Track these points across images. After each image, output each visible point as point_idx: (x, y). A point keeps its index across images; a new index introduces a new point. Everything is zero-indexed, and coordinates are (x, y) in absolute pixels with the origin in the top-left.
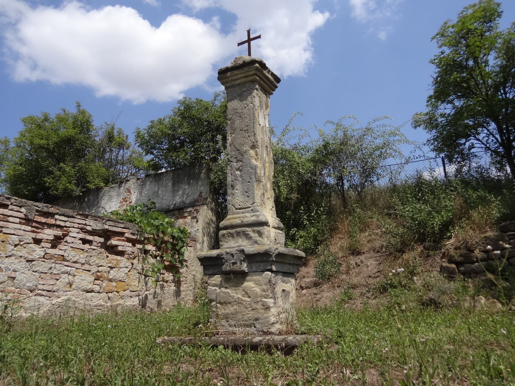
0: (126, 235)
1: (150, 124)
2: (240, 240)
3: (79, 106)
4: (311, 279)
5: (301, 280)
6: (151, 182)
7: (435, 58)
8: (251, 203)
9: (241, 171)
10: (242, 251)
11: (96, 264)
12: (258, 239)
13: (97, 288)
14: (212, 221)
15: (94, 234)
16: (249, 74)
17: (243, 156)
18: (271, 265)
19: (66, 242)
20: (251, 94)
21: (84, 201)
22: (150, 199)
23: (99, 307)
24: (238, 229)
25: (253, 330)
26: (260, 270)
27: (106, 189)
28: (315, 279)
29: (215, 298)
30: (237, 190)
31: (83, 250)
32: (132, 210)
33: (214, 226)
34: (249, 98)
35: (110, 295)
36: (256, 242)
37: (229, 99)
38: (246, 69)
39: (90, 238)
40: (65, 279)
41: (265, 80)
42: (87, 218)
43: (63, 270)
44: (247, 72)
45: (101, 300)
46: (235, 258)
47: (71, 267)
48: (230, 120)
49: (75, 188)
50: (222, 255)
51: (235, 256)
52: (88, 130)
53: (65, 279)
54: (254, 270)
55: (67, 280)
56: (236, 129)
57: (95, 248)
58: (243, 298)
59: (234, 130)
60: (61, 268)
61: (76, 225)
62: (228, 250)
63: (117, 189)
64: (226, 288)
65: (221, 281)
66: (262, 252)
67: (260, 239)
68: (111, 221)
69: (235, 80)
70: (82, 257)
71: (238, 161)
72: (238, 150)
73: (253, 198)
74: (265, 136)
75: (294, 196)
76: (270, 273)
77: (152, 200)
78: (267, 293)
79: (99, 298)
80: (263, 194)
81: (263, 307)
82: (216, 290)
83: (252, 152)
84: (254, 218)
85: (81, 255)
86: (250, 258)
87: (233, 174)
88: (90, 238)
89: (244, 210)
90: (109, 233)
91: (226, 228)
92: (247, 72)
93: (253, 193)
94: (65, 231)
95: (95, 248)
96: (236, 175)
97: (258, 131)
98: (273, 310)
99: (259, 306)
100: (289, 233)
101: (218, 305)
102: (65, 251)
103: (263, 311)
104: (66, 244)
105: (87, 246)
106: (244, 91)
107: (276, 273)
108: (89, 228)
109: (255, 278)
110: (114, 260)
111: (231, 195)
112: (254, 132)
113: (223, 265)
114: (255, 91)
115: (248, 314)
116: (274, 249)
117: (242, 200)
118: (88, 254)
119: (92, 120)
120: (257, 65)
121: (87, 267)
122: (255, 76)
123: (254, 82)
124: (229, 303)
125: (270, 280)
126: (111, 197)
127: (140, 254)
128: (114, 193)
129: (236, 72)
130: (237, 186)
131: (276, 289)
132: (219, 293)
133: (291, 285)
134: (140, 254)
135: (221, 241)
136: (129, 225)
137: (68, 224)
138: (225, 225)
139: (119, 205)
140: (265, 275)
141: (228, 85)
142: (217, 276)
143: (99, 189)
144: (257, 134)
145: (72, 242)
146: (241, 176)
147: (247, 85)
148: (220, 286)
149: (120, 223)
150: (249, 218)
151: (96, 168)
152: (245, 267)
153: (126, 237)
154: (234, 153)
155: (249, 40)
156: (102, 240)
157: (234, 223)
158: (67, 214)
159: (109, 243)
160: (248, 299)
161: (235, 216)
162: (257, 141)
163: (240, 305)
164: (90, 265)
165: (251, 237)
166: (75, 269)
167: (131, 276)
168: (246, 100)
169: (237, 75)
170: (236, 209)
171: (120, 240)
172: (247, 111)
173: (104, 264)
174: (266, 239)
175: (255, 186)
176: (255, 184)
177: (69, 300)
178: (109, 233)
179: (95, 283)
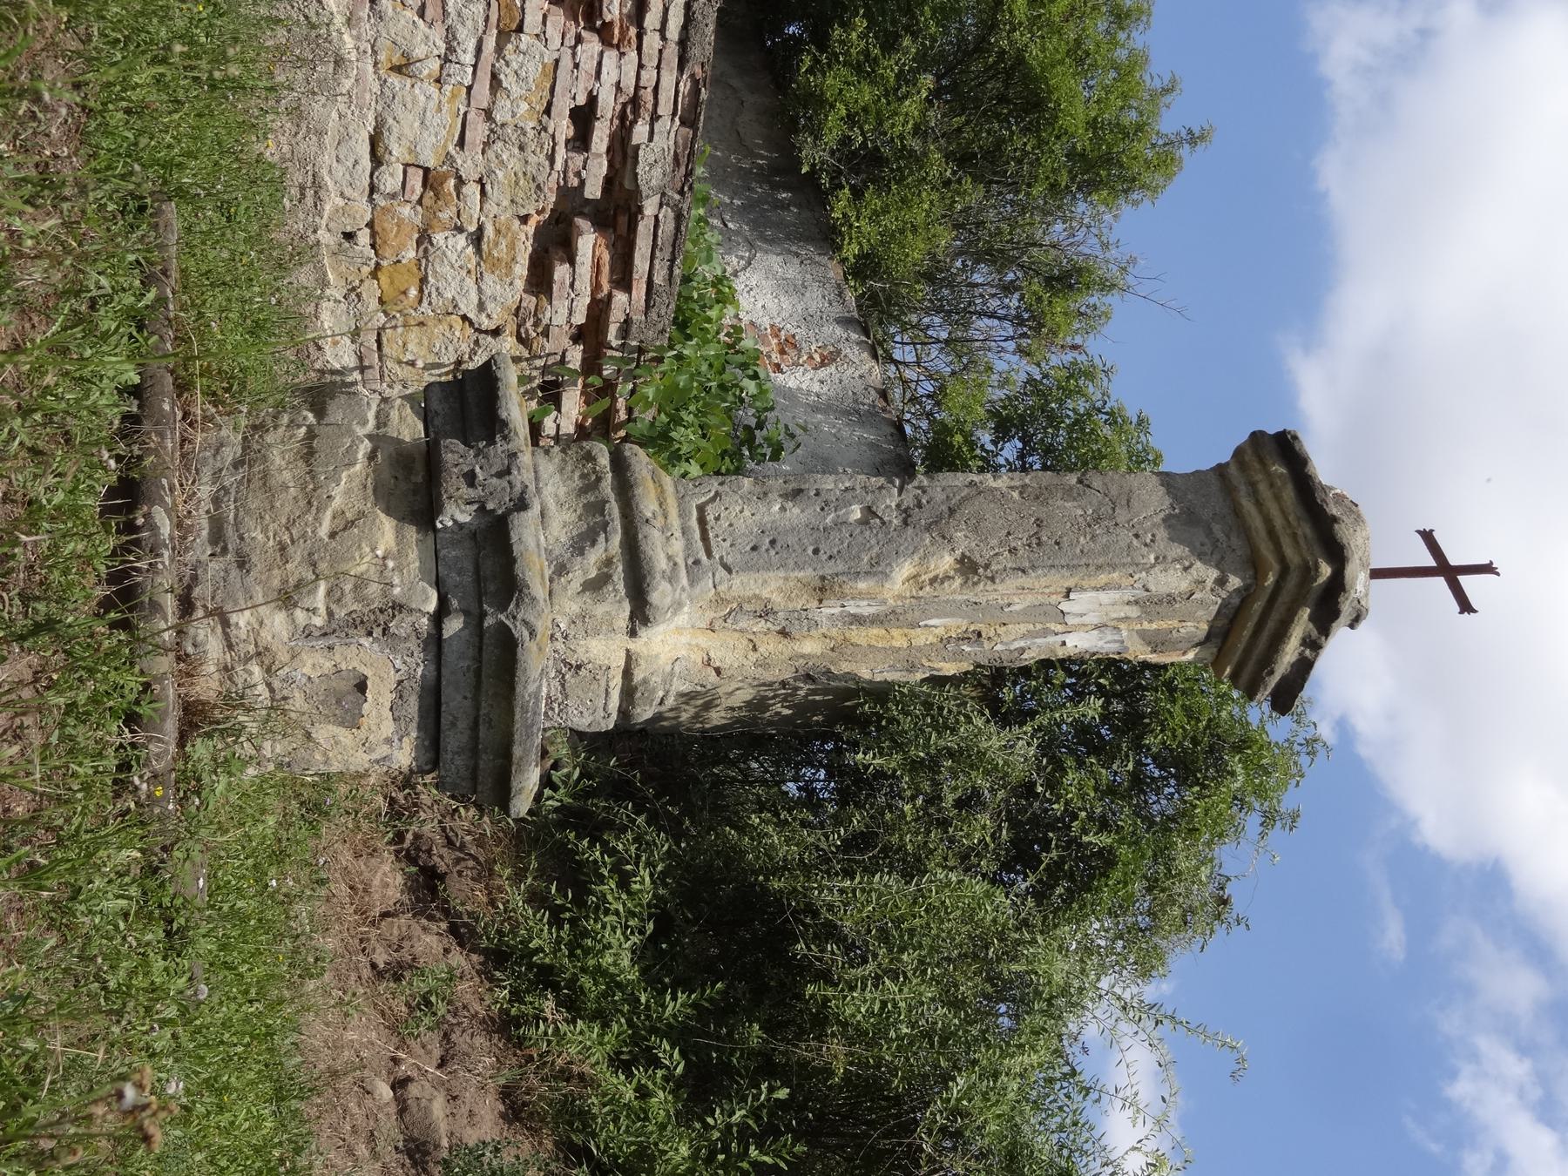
0: (620, 298)
1: (1131, 414)
2: (569, 516)
3: (1193, 139)
4: (443, 1128)
5: (438, 1084)
6: (872, 445)
8: (729, 560)
9: (864, 522)
10: (521, 505)
11: (491, 172)
12: (576, 579)
13: (390, 180)
14: (708, 706)
15: (618, 159)
17: (928, 528)
18: (466, 613)
19: (579, 39)
20: (1201, 556)
21: (776, 187)
22: (792, 436)
23: (310, 193)
24: (614, 509)
25: (200, 548)
27: (835, 271)
28: (445, 1143)
29: (330, 419)
30: (783, 509)
31: (548, 111)
32: (740, 358)
33: (684, 716)
34: (1178, 550)
35: (364, 238)
36: (561, 569)
37: (1167, 480)
38: (1306, 529)
39: (600, 138)
40: (426, 43)
41: (1271, 625)
42: (683, 123)
43: (462, 33)
44: (1294, 536)
45: (340, 202)
46: (495, 480)
47: (475, 66)
48: (1080, 481)
49: (831, 137)
50: (505, 438)
52: (1090, 187)
53: (426, 43)
54: (442, 553)
55: (419, 52)
56: (1045, 503)
57: (559, 165)
58: (329, 514)
60: (469, 23)
61: (648, 77)
63: (837, 310)
64: (371, 457)
65: (399, 441)
67: (576, 586)
68: (678, 229)
70: (517, 108)
71: (905, 511)
72: (952, 511)
73: (748, 567)
74: (1023, 628)
75: (836, 1054)
76: (432, 606)
77: (789, 445)
78: (349, 598)
79: (348, 192)
80: (766, 613)
81: (292, 582)
82: (364, 423)
83: (945, 562)
84: (661, 564)
85: (524, 106)
86: (493, 537)
87: (849, 495)
88: (600, 138)
89: (697, 535)
90: (623, 220)
91: (620, 465)
92: (1294, 536)
93: (769, 567)
94: (623, 32)
95: (559, 165)
97: (1046, 584)
98: (277, 624)
99: (296, 569)
100: (663, 1035)
101: (303, 430)
102: (541, 36)
103: (276, 583)
104: (570, 41)
105: (564, 128)
106: (1209, 532)
107: (435, 643)
108: (640, 132)
109: (413, 555)
110: (512, 246)
111: (758, 489)
112: (1034, 567)
113: (466, 444)
114: (1213, 574)
115: (265, 530)
116: (531, 618)
117: (740, 525)
118: (531, 134)
119: (1136, 203)
120: (1326, 570)
121: (478, 131)
122: (1276, 567)
123: (1254, 566)
125: (401, 606)
126: (799, 290)
127: (539, 363)
128: (816, 299)
129: (1289, 494)
131: (366, 642)
132: (350, 432)
133: (389, 741)
134: (539, 363)
136: (666, 309)
137: (652, 41)
138: (633, 461)
139: (765, 322)
140: (424, 590)
141: (1233, 470)
142: (421, 426)
143: (828, 237)
144: (1022, 580)
145: (577, 66)
146: (840, 524)
147: (1236, 542)
149: (671, 269)
150: (665, 548)
151: (918, 224)
152: (456, 514)
153: (610, 296)
154: (939, 496)
155: (1449, 573)
156: (594, 191)
157: (638, 491)
158: (695, 37)
159: (583, 223)
160: (323, 531)
161: (672, 503)
162: (992, 579)
163: (302, 503)
164: (487, 144)
165: (581, 552)
166: (467, 81)
167: (443, 327)
168: (1171, 539)
170: (701, 509)
171: (598, 273)
172: (1123, 544)
173: (490, 207)
174: (574, 607)
175: (801, 574)
176: (807, 574)
177: (339, 62)
178: (623, 220)
179: (411, 170)
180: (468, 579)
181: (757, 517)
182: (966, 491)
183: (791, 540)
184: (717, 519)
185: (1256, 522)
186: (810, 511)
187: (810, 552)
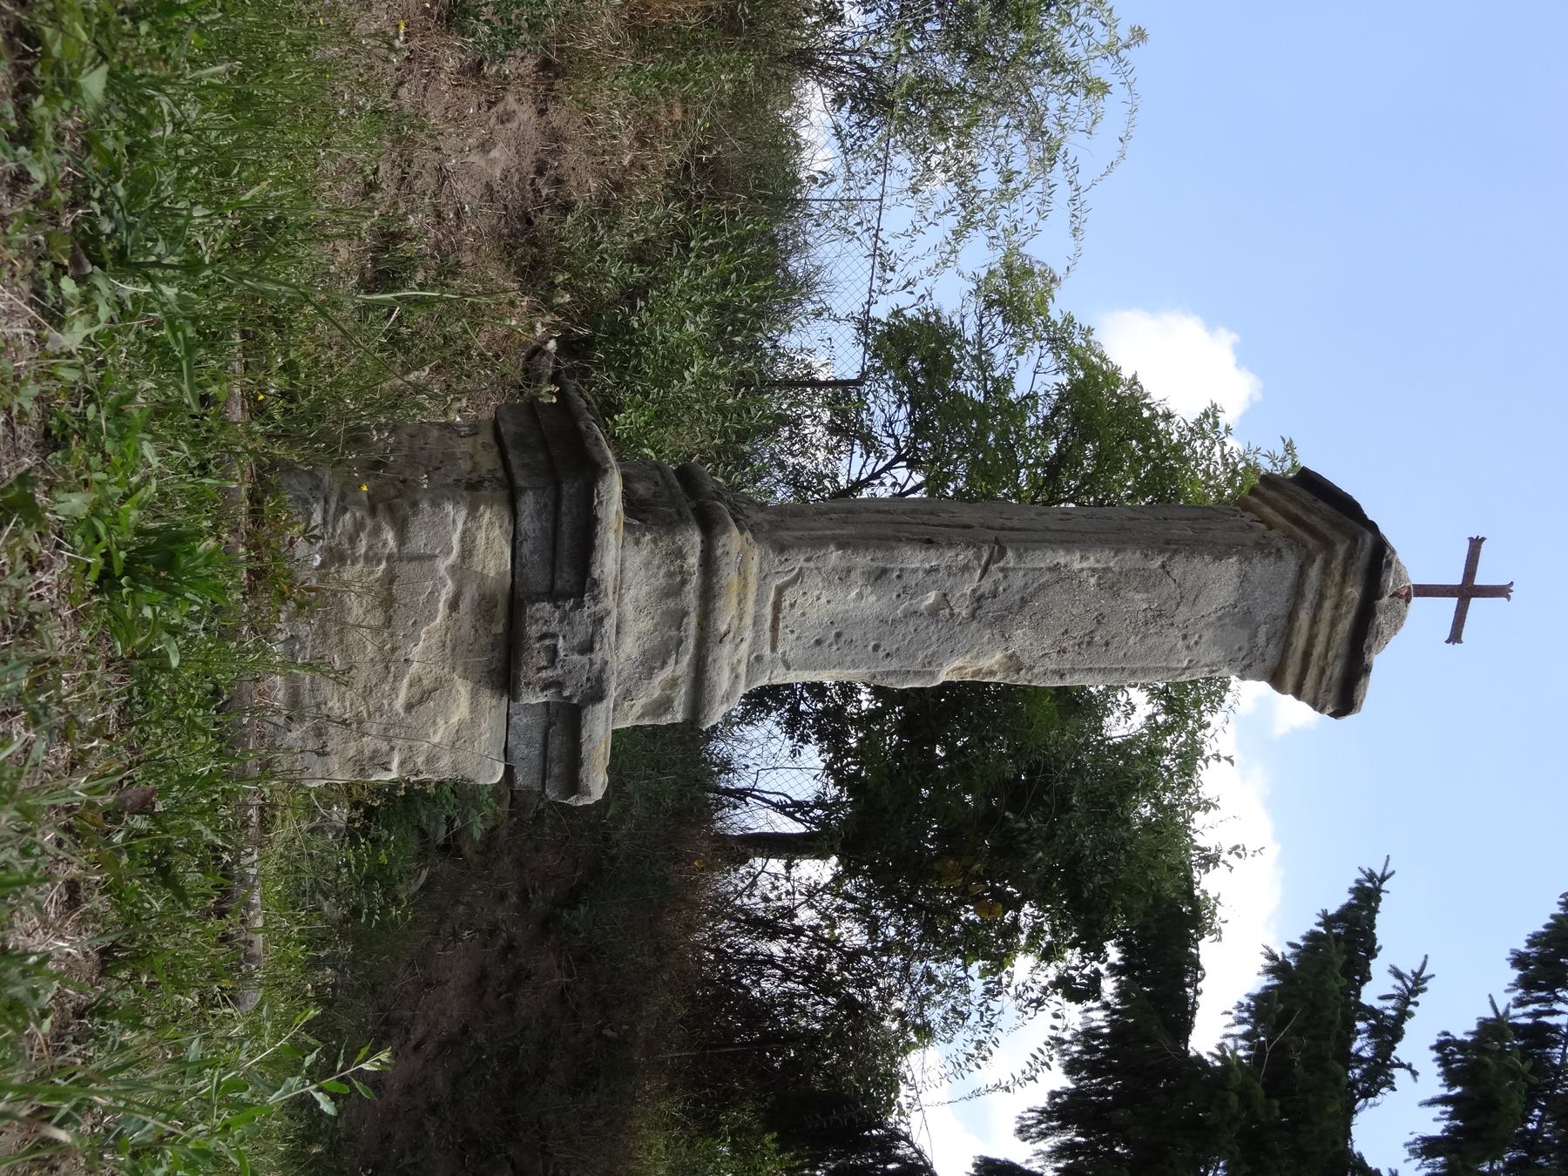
7: (1222, 428)
8: (790, 656)
9: (934, 611)
16: (1313, 673)
17: (991, 625)
24: (692, 621)
26: (512, 742)
30: (860, 596)
38: (1336, 670)
44: (1322, 672)
46: (576, 657)
48: (1163, 566)
51: (585, 659)
54: (514, 719)
58: (406, 681)
59: (1111, 585)
62: (610, 624)
66: (583, 775)
69: (1318, 607)
81: (367, 753)
87: (929, 580)
89: (768, 624)
92: (1322, 672)
96: (922, 589)
117: (813, 615)
124: (389, 621)
130: (873, 598)
135: (655, 541)
148: (461, 570)
157: (720, 603)
160: (399, 704)
163: (379, 667)
169: (1333, 624)
170: (780, 591)
180: (535, 752)
181: (832, 605)
182: (1047, 576)
183: (857, 634)
184: (792, 606)
185: (1299, 643)
186: (885, 600)
187: (870, 648)
